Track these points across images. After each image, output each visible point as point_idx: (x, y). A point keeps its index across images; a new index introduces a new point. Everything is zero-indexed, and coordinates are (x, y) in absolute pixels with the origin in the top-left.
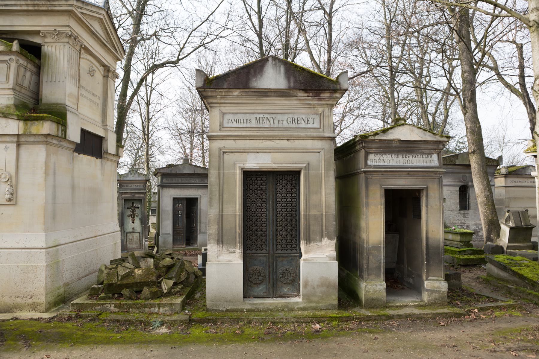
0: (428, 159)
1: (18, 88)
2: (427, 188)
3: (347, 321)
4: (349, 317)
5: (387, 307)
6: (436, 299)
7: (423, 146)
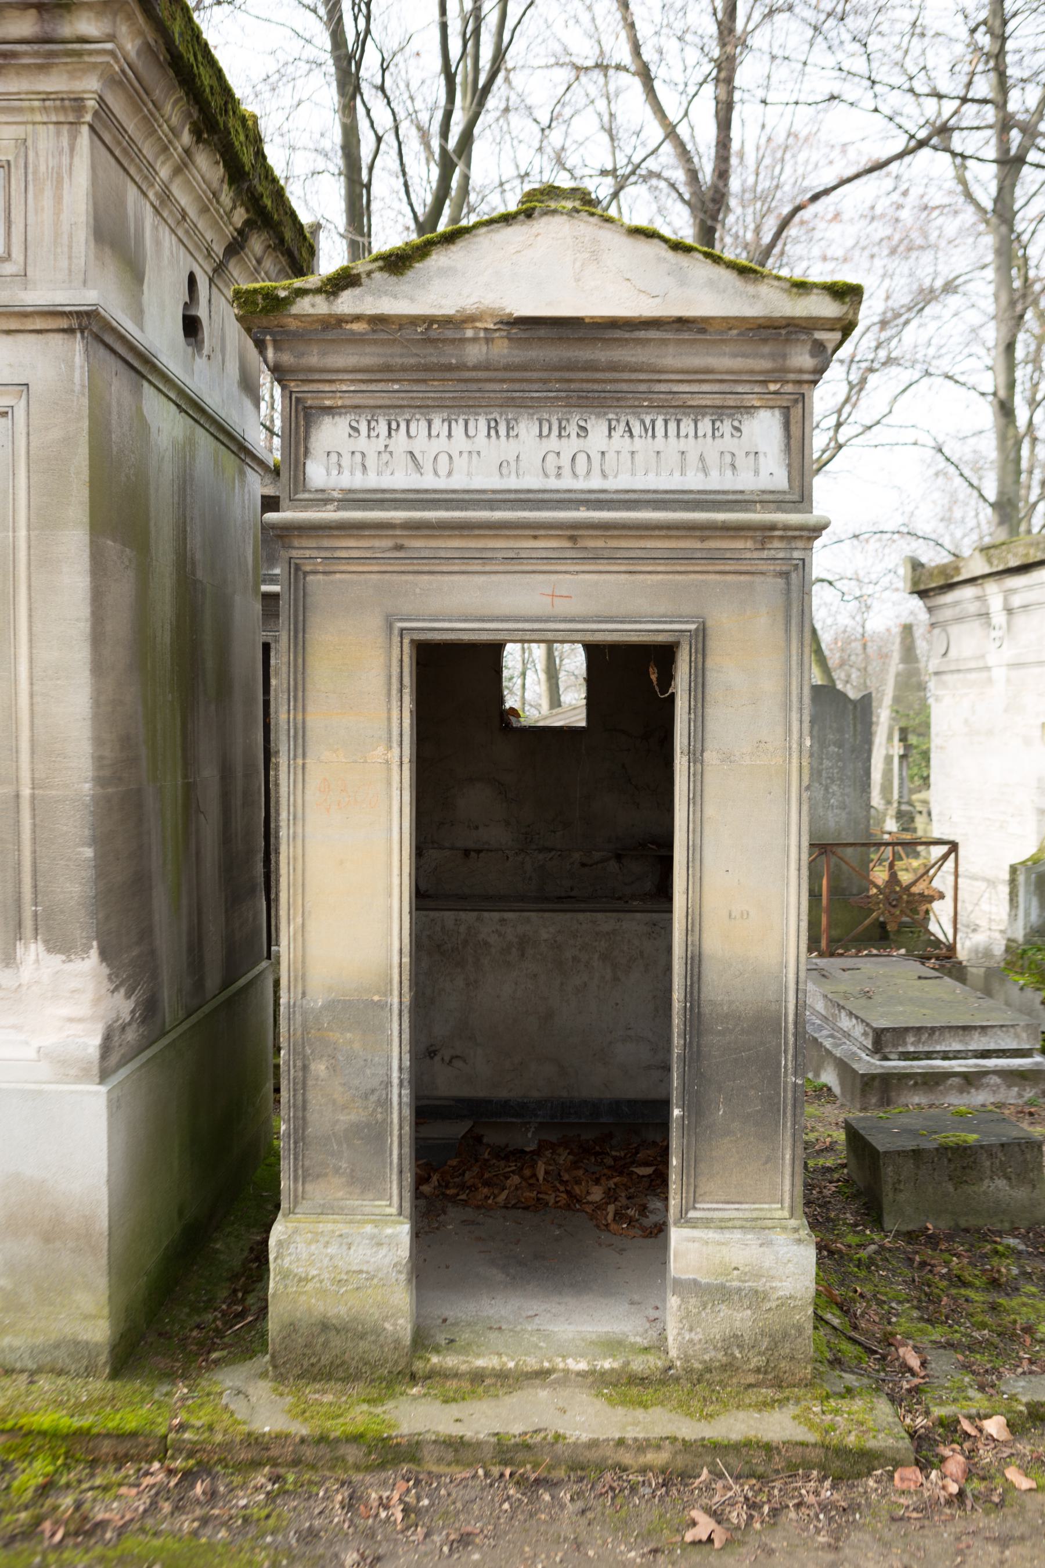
0: (711, 448)
1: (502, 429)
2: (701, 636)
3: (121, 1460)
4: (133, 1435)
5: (413, 1378)
6: (736, 1340)
7: (675, 357)
